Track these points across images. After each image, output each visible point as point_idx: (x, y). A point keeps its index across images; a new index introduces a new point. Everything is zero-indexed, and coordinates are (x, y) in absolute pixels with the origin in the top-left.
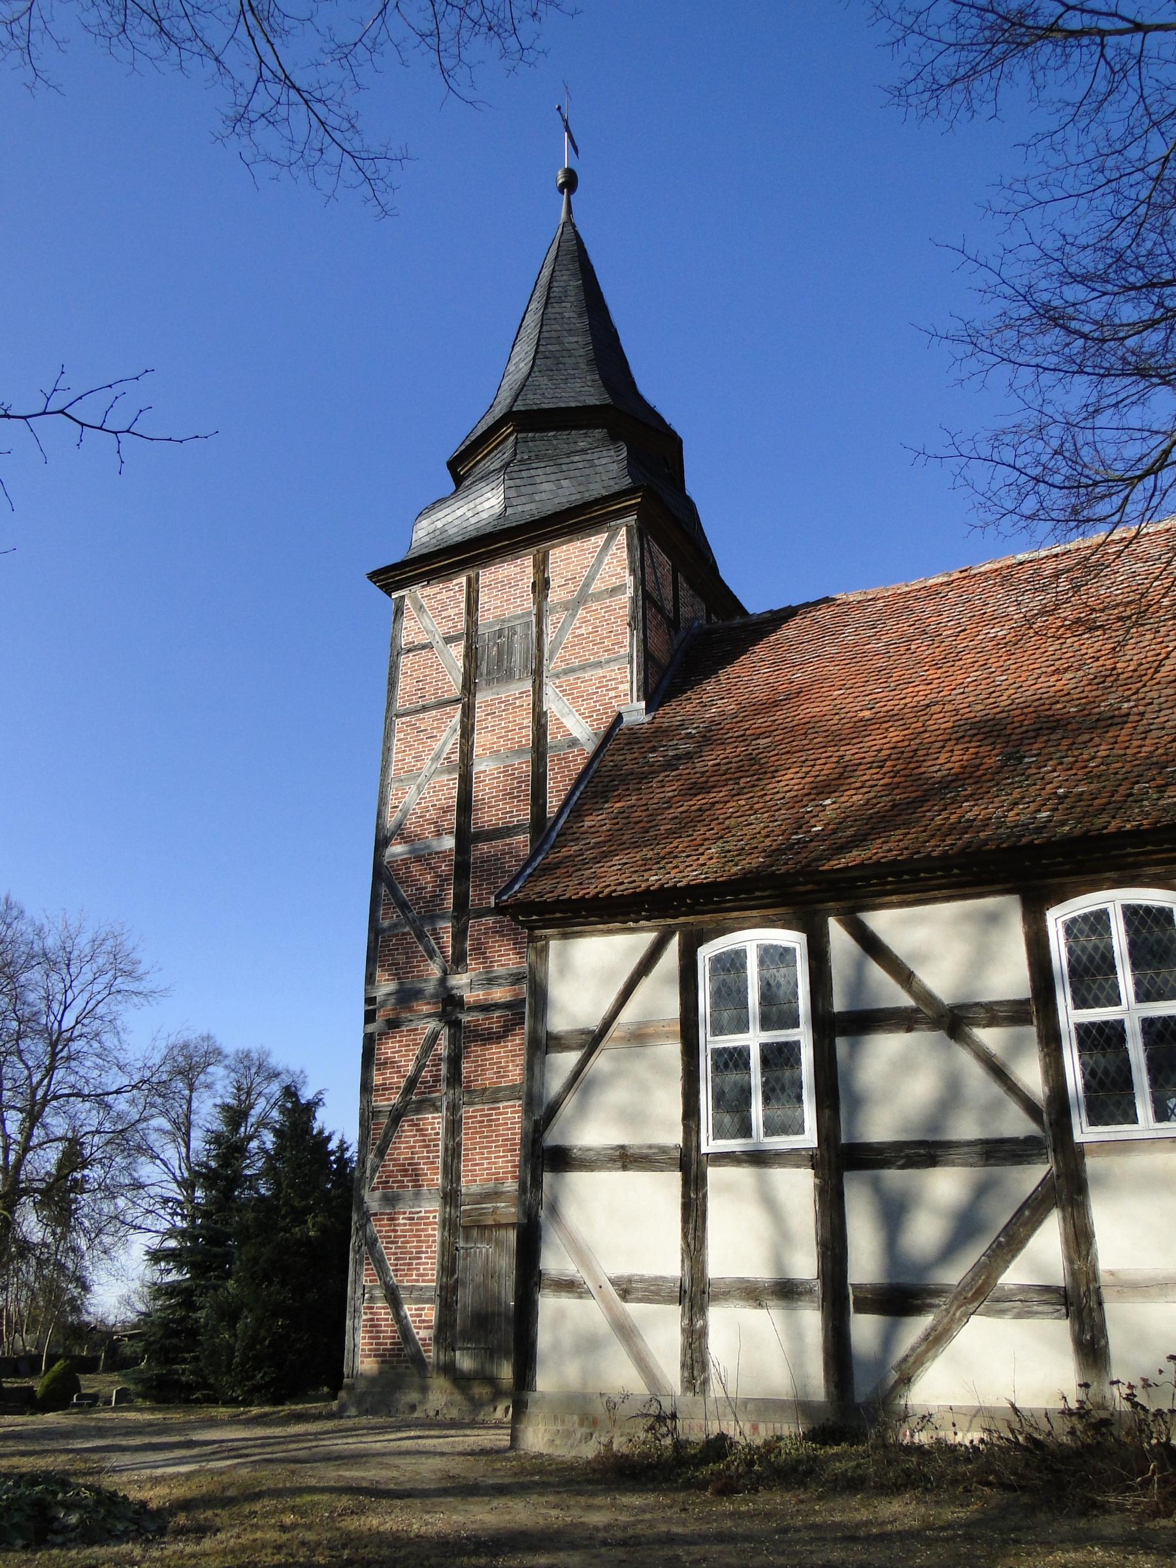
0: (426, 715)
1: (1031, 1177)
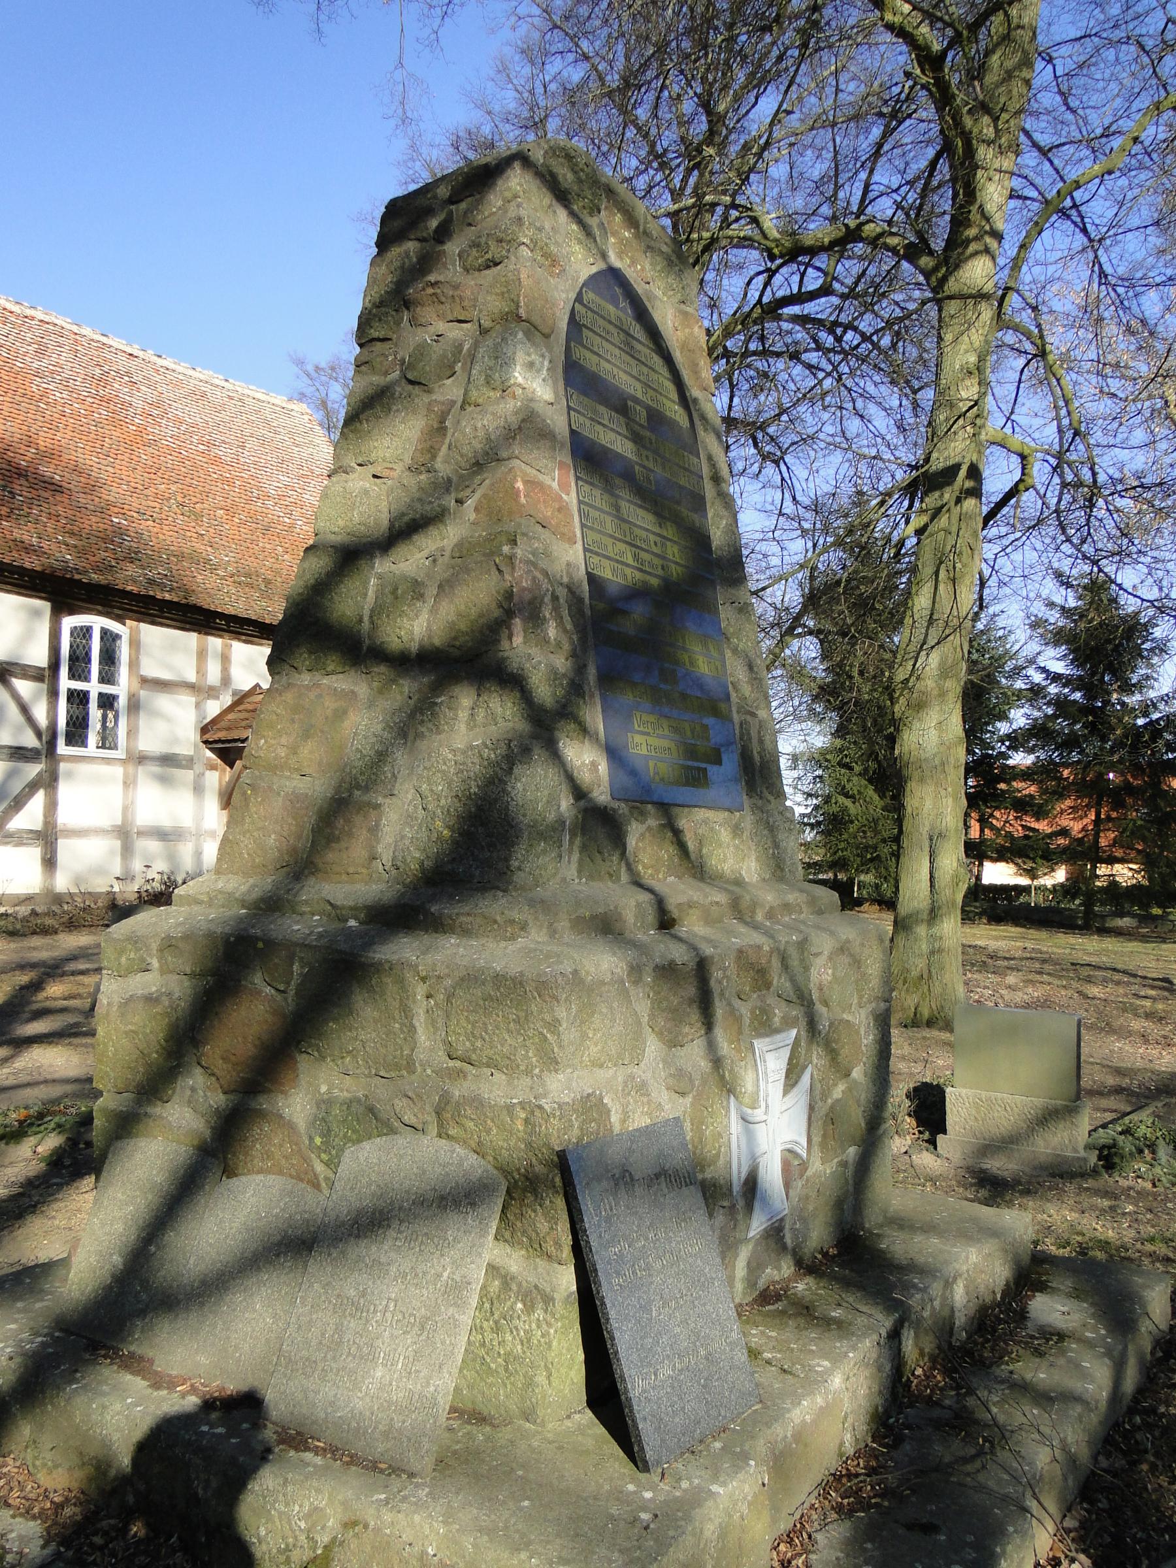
1: (33, 770)
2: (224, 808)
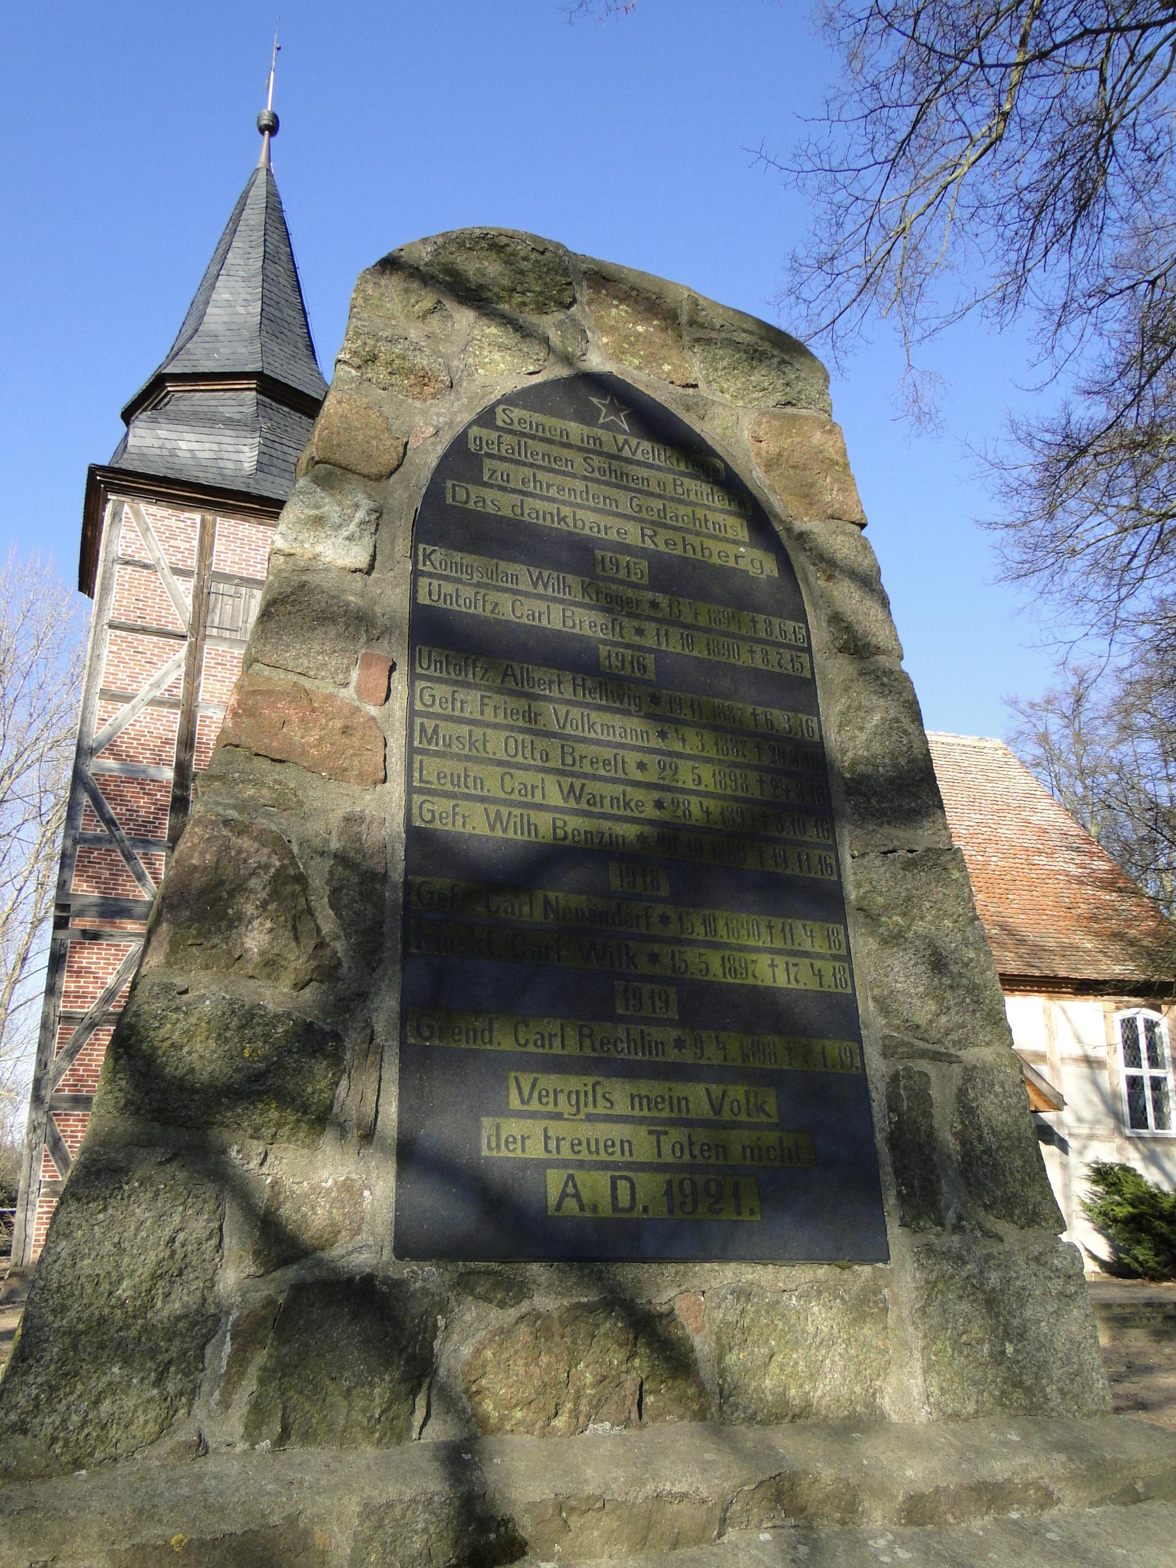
0: (146, 638)
2: (268, 1212)
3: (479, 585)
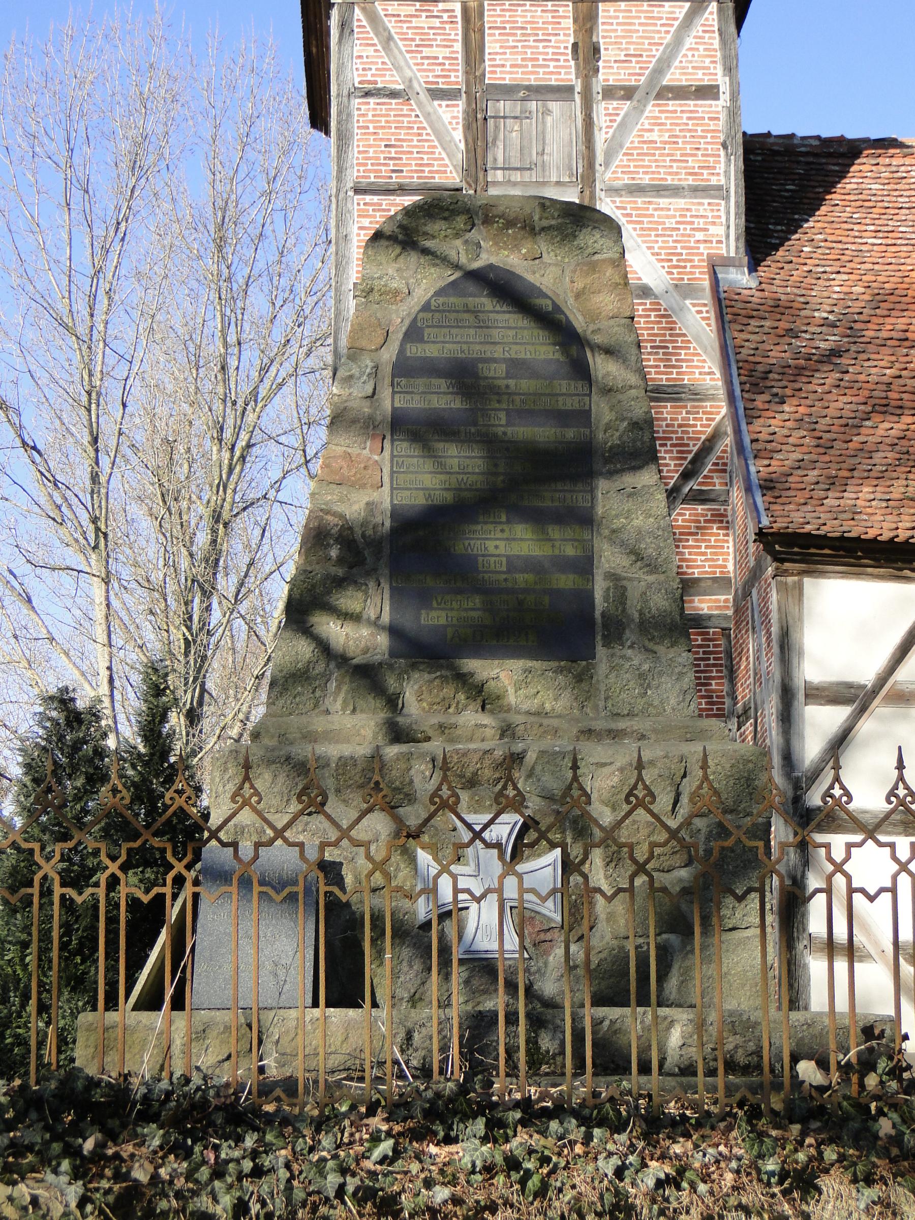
3: (423, 393)
